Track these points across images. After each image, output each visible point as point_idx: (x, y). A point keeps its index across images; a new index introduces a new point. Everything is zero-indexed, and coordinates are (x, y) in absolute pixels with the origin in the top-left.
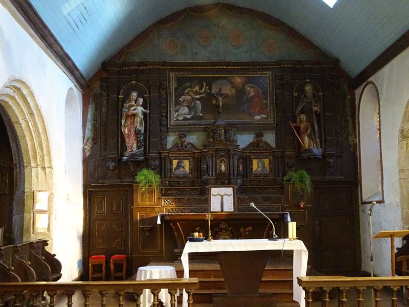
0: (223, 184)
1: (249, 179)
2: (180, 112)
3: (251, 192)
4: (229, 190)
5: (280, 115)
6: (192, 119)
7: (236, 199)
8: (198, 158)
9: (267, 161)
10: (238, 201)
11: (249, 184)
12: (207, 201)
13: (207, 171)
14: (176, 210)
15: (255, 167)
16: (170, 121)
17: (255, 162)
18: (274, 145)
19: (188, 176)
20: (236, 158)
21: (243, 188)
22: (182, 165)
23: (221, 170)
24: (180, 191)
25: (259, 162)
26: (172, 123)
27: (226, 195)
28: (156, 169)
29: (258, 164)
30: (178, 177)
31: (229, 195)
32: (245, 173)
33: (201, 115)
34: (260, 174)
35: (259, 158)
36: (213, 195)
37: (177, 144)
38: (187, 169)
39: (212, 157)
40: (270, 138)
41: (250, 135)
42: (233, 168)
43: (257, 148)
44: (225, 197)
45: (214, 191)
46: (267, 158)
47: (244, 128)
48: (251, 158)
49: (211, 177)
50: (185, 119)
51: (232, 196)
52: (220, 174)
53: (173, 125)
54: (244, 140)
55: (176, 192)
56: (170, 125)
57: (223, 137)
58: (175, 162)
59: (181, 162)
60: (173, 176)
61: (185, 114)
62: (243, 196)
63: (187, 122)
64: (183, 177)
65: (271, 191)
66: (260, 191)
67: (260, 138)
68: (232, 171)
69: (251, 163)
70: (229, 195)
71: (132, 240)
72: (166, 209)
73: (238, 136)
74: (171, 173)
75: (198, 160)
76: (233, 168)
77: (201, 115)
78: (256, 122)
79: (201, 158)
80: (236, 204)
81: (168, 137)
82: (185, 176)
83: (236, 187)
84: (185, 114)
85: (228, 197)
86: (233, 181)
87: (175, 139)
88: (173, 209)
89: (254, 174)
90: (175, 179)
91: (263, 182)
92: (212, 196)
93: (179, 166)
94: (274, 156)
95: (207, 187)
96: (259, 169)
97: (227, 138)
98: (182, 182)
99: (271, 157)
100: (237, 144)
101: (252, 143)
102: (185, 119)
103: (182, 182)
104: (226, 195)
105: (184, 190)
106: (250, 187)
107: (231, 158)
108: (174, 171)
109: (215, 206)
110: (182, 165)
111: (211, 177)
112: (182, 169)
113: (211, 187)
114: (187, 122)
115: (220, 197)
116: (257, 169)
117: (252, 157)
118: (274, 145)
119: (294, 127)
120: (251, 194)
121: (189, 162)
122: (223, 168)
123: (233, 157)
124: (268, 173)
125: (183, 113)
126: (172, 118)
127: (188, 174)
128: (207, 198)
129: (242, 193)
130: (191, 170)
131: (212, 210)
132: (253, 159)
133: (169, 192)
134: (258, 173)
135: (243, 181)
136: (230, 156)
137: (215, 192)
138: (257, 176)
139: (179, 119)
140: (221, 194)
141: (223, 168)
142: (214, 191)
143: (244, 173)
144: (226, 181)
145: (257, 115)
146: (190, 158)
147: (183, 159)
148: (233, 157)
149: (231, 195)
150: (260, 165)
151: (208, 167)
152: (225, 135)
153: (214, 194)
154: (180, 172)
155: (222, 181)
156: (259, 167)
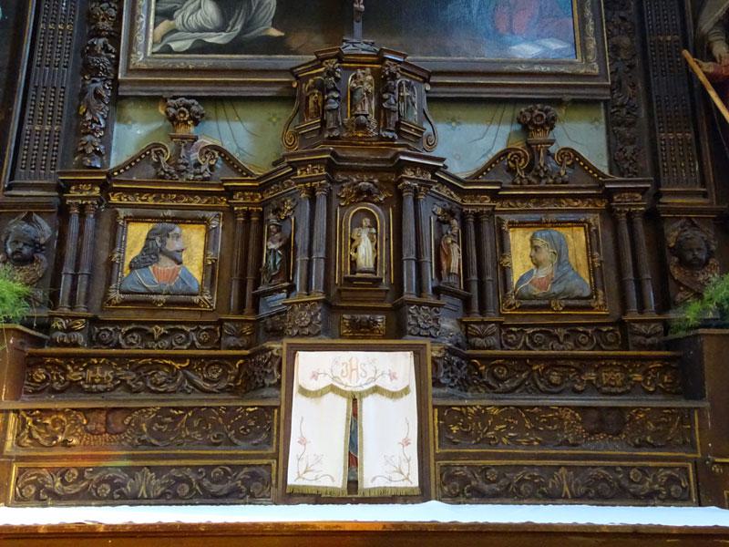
0: (361, 335)
1: (492, 316)
2: (178, 21)
3: (508, 384)
4: (396, 367)
5: (626, 41)
6: (234, 47)
7: (434, 421)
8: (248, 214)
9: (576, 239)
10: (444, 429)
11: (493, 340)
12: (269, 426)
13: (286, 270)
14: (81, 477)
15: (519, 263)
16: (130, 51)
17: (519, 241)
18: (602, 164)
19: (196, 299)
20: (431, 210)
21: (469, 358)
22: (172, 245)
23: (354, 263)
24: (136, 369)
25: (539, 243)
26: (139, 59)
27: (376, 390)
28: (29, 260)
29: (535, 248)
30: (141, 301)
31: (394, 395)
32: (475, 287)
33: (275, 33)
34: (547, 297)
35: (539, 223)
36: (304, 392)
37: (156, 148)
38: (194, 267)
39: (313, 200)
40: (583, 137)
41: (493, 128)
42: (419, 253)
43: (526, 181)
44: (369, 406)
45: (313, 367)
46: (578, 223)
47: (468, 94)
48: (500, 222)
49: (301, 300)
50: (201, 48)
51: (412, 398)
52: (348, 281)
53: (140, 71)
54: (468, 144)
55: (108, 373)
56: (129, 71)
57: (368, 107)
58: (137, 235)
59: (165, 234)
60: (116, 296)
61: (202, 29)
62: (474, 401)
63: (207, 60)
64: (168, 303)
65: (618, 376)
66: (555, 378)
67: (539, 136)
68: (410, 270)
69: (503, 247)
70: (394, 395)
71: (664, 392)
72: (21, 471)
73: (441, 128)
74: (109, 283)
75: (247, 209)
76: (419, 253)
77: (275, 33)
78: (523, 68)
79: (261, 215)
80: (435, 448)
81: (117, 128)
82: (180, 301)
83: (433, 351)
84: (202, 29)
85: (389, 402)
86: (415, 317)
87: (151, 133)
88: (63, 473)
89: (519, 297)
90: (131, 314)
91: (561, 332)
92: (298, 400)
93: (152, 253)
94: (610, 214)
95: (276, 346)
96: (542, 274)
97: (389, 111)
98: (162, 330)
99: (594, 219)
100: (437, 153)
101: (504, 154)
102: (201, 48)
103: (162, 330)
104: (376, 390)
105: (158, 367)
106: (498, 352)
107: (409, 203)
108: (127, 271)
109: (313, 449)
110: (172, 245)
111: (301, 300)
112: (166, 265)
113: (294, 350)
114: (207, 60)
115: (342, 405)
116: (530, 273)
117: (507, 218)
118: (602, 164)
119: (709, 76)
120: (512, 391)
121: (208, 232)
122: (365, 253)
123: (416, 201)
124: (587, 293)
125: (192, 22)
126: (140, 39)
127: (195, 288)
128: (269, 409)
129: (464, 385)
130: (210, 269)
131: (292, 480)
132: (513, 225)
133: (74, 375)
134: (537, 292)
135: (465, 325)
136: (399, 194)
137: (315, 376)
138: (530, 304)
139: (174, 46)
140: (354, 384)
141: (365, 253)
142: (313, 367)
143: (467, 286)
144: (380, 319)
145: (526, 40)
146: (210, 215)
147: (178, 220)
148: (416, 201)
149: (406, 391)
150: (546, 254)
151: (287, 247)
152: (380, 100)
153: (312, 385)
154: (159, 276)
155: (361, 316)
156: (537, 264)
